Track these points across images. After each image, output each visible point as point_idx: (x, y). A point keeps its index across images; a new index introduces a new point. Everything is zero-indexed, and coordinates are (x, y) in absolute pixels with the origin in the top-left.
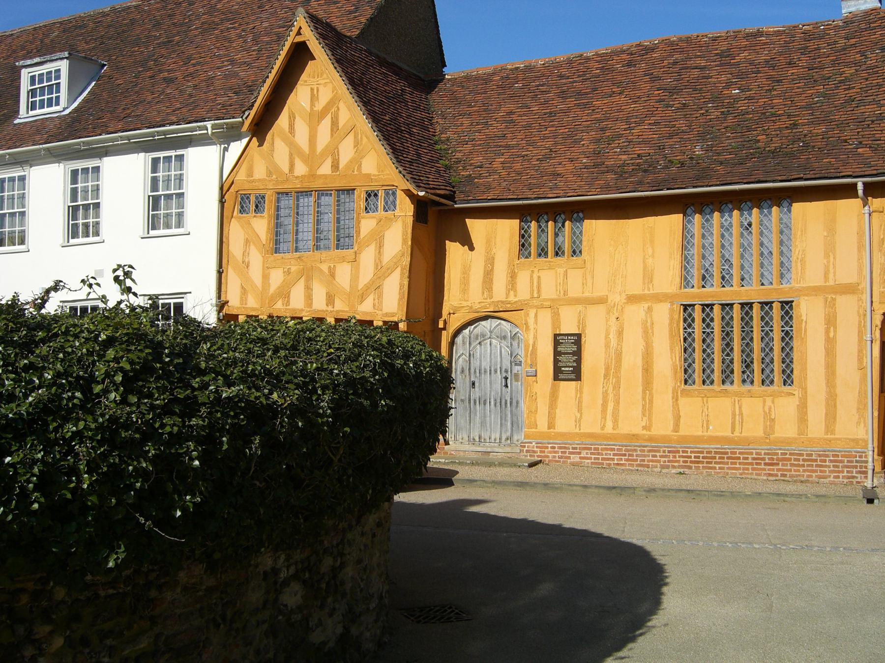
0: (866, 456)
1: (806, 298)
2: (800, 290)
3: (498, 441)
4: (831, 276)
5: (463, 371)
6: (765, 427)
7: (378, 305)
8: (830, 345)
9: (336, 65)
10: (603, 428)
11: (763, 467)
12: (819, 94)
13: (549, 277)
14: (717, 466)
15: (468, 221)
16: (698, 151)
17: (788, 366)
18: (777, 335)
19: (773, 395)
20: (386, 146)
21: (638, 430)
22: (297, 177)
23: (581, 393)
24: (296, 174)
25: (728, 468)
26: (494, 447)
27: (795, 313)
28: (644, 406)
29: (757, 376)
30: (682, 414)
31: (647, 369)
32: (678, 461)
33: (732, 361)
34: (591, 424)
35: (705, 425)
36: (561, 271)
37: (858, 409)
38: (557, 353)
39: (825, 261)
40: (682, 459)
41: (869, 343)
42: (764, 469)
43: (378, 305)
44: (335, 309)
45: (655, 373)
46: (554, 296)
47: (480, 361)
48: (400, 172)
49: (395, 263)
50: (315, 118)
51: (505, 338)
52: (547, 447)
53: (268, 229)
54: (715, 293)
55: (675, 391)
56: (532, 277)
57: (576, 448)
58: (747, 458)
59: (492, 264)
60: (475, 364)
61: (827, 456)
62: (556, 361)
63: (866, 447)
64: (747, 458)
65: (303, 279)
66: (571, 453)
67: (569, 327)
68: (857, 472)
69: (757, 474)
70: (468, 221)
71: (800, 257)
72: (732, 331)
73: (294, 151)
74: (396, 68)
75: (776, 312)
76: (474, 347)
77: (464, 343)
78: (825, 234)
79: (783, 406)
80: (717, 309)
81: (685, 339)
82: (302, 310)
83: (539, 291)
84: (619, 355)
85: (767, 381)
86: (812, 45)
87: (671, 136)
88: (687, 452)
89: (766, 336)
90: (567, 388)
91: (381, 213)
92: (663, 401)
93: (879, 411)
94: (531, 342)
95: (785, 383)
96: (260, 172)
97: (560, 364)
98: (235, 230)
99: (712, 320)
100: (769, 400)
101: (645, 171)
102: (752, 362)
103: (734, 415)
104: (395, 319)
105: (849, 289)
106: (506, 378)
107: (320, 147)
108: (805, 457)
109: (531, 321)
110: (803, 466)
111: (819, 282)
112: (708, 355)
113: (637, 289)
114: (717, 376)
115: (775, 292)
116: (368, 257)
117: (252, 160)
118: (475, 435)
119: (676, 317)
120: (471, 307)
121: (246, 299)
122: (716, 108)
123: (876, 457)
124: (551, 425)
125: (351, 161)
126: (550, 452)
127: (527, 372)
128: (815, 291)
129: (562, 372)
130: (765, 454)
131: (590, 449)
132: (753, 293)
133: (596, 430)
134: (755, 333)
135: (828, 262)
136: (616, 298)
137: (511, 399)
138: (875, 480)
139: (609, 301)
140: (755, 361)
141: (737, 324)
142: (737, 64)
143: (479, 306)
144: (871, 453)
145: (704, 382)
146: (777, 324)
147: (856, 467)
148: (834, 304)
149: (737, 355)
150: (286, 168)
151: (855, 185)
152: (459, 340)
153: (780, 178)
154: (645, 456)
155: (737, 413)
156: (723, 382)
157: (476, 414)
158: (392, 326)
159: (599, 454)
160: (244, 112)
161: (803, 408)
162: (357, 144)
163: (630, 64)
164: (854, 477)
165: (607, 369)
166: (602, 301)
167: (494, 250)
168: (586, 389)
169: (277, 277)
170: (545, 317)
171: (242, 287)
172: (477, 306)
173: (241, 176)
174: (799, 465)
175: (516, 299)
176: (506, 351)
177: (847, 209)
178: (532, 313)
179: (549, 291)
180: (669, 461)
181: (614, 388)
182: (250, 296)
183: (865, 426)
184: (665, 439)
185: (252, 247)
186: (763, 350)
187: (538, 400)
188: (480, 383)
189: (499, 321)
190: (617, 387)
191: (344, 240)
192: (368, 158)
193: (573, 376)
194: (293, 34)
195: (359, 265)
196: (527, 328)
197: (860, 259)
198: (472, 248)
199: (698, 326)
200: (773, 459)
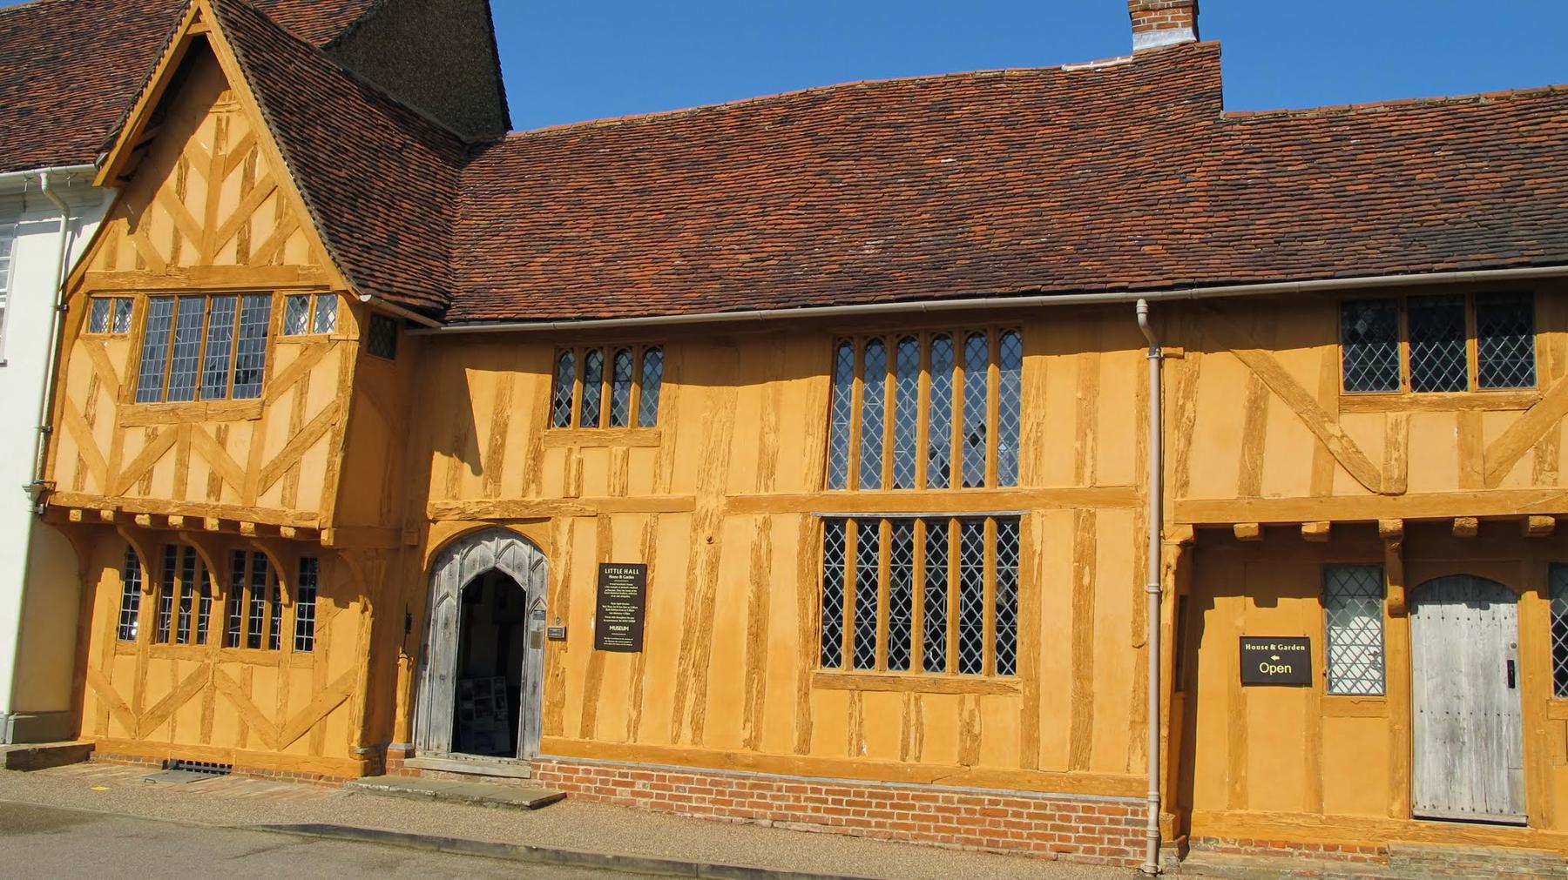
0: (1145, 813)
1: (1042, 511)
2: (1031, 497)
7: (288, 499)
8: (1083, 597)
9: (248, 72)
10: (676, 739)
12: (1084, 164)
13: (596, 462)
14: (873, 821)
17: (1007, 637)
19: (981, 690)
20: (315, 214)
21: (736, 747)
22: (182, 270)
24: (181, 265)
31: (757, 635)
32: (804, 809)
36: (618, 450)
38: (602, 599)
39: (1078, 445)
41: (1153, 598)
42: (958, 831)
43: (288, 499)
44: (222, 502)
46: (606, 497)
50: (219, 169)
52: (577, 771)
54: (883, 499)
55: (804, 676)
56: (568, 459)
57: (626, 775)
59: (503, 435)
61: (1074, 809)
62: (600, 614)
65: (175, 448)
66: (617, 783)
67: (626, 552)
68: (1127, 843)
74: (401, 108)
75: (989, 537)
77: (451, 574)
79: (998, 709)
80: (884, 528)
81: (827, 582)
82: (169, 503)
83: (578, 486)
84: (710, 601)
86: (1079, 94)
87: (829, 226)
90: (618, 663)
93: (1170, 728)
94: (560, 578)
95: (1001, 669)
97: (607, 619)
98: (80, 360)
100: (970, 702)
102: (944, 629)
104: (315, 525)
105: (1123, 497)
107: (223, 217)
108: (1032, 810)
109: (563, 540)
110: (1028, 826)
111: (1068, 484)
115: (988, 500)
116: (281, 412)
117: (116, 239)
119: (811, 540)
122: (911, 185)
123: (1163, 813)
124: (587, 731)
125: (268, 244)
128: (1059, 498)
131: (649, 777)
132: (952, 500)
133: (665, 743)
134: (949, 573)
135: (1084, 446)
136: (711, 503)
140: (948, 626)
141: (918, 556)
142: (957, 122)
144: (1153, 808)
146: (989, 557)
147: (1126, 833)
148: (1093, 525)
151: (1133, 305)
153: (998, 290)
158: (309, 536)
159: (664, 788)
161: (1031, 714)
162: (279, 215)
163: (785, 120)
164: (1122, 852)
165: (688, 632)
167: (508, 411)
168: (648, 669)
169: (135, 442)
170: (587, 531)
173: (97, 266)
175: (540, 499)
178: (565, 528)
179: (596, 488)
180: (787, 808)
182: (90, 475)
184: (782, 765)
191: (249, 378)
193: (628, 642)
194: (186, 21)
196: (556, 551)
199: (850, 556)
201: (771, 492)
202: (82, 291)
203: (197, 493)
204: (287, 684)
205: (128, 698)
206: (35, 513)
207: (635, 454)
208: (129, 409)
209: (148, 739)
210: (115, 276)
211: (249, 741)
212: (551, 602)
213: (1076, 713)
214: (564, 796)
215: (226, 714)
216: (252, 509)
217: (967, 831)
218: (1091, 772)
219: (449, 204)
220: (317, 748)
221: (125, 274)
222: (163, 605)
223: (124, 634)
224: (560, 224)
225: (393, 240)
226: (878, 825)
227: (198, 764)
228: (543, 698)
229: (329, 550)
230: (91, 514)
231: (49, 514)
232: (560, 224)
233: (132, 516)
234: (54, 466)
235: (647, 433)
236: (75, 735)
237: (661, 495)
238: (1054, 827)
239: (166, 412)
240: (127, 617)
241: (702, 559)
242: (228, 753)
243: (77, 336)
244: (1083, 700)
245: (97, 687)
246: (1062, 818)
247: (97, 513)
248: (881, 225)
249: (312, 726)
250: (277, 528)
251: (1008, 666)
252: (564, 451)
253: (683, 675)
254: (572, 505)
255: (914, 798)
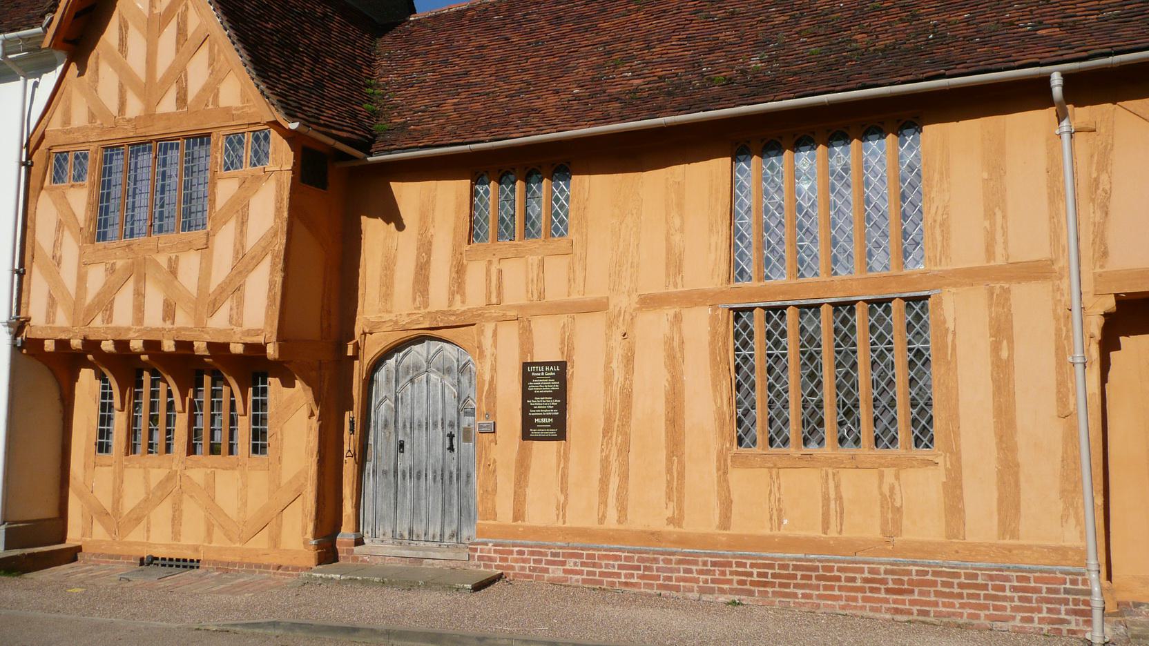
1: (953, 290)
3: (438, 539)
4: (999, 249)
5: (386, 426)
6: (884, 523)
8: (1002, 373)
10: (602, 520)
11: (883, 595)
13: (516, 272)
14: (800, 592)
15: (394, 186)
16: (755, 62)
17: (922, 412)
18: (900, 357)
19: (897, 465)
20: (242, 51)
22: (129, 121)
23: (566, 459)
25: (820, 597)
26: (429, 549)
27: (930, 317)
28: (669, 483)
29: (867, 431)
30: (735, 496)
31: (674, 420)
32: (730, 582)
33: (819, 405)
34: (582, 514)
35: (775, 517)
36: (534, 259)
37: (1063, 492)
38: (527, 395)
39: (987, 224)
40: (736, 578)
42: (887, 601)
44: (176, 326)
45: (688, 424)
47: (413, 408)
48: (258, 86)
49: (264, 248)
51: (448, 371)
52: (511, 552)
53: (89, 203)
55: (721, 458)
56: (488, 271)
57: (556, 555)
58: (853, 580)
60: (404, 413)
61: (1007, 579)
62: (526, 408)
63: (1083, 562)
64: (853, 580)
65: (132, 279)
66: (549, 563)
67: (546, 351)
68: (1067, 612)
69: (872, 609)
70: (394, 186)
71: (939, 219)
72: (818, 353)
73: (126, 80)
76: (404, 387)
77: (388, 380)
78: (985, 175)
79: (918, 484)
81: (738, 368)
82: (129, 329)
83: (499, 294)
84: (627, 397)
85: (886, 439)
87: (711, 51)
88: (744, 565)
89: (880, 359)
90: (545, 451)
91: (247, 169)
92: (702, 473)
94: (487, 377)
96: (79, 118)
97: (532, 413)
99: (783, 334)
101: (669, 94)
102: (856, 406)
103: (826, 499)
104: (260, 340)
105: (1038, 271)
106: (451, 436)
107: (161, 70)
108: (963, 580)
109: (487, 342)
110: (960, 596)
111: (977, 260)
112: (778, 395)
113: (655, 284)
114: (794, 430)
116: (224, 240)
117: (69, 99)
118: (403, 528)
119: (722, 329)
120: (396, 323)
121: (54, 314)
122: (782, 12)
124: (518, 515)
125: (204, 90)
126: (516, 561)
127: (480, 426)
128: (970, 276)
129: (535, 426)
130: (886, 572)
131: (580, 556)
133: (591, 523)
135: (993, 225)
136: (623, 302)
137: (459, 470)
138: (1107, 629)
139: (611, 307)
140: (862, 404)
143: (407, 320)
145: (771, 442)
146: (899, 338)
147: (1066, 602)
148: (1007, 299)
149: (828, 394)
150: (113, 108)
151: (1046, 80)
152: (381, 375)
154: (671, 570)
155: (832, 495)
156: (806, 441)
157: (405, 494)
159: (594, 565)
160: (43, 17)
161: (954, 489)
164: (1062, 621)
165: (609, 420)
166: (599, 306)
167: (432, 231)
168: (574, 456)
169: (97, 278)
170: (510, 335)
171: (51, 296)
172: (404, 321)
173: (55, 124)
174: (951, 595)
176: (451, 391)
177: (1026, 128)
178: (489, 328)
179: (515, 294)
180: (713, 581)
181: (620, 452)
183: (1078, 523)
184: (705, 540)
185: (67, 234)
186: (875, 384)
187: (498, 472)
188: (412, 445)
189: (441, 344)
190: (624, 450)
191: (191, 215)
192: (229, 88)
193: (553, 433)
195: (211, 253)
196: (482, 354)
197: (1054, 216)
198: (400, 227)
199: (759, 345)
200: (901, 582)
201: (680, 289)
202: (43, 147)
203: (154, 318)
204: (245, 486)
205: (107, 503)
206: (14, 347)
207: (549, 262)
208: (90, 248)
209: (126, 539)
210: (70, 132)
211: (215, 537)
212: (480, 400)
213: (1002, 483)
214: (500, 577)
215: (193, 515)
216: (203, 329)
217: (895, 602)
218: (1023, 542)
219: (369, 66)
220: (275, 541)
221: (79, 129)
222: (133, 421)
223: (103, 448)
224: (466, 74)
225: (319, 84)
226: (804, 596)
227: (171, 560)
228: (477, 487)
229: (275, 362)
230: (62, 344)
231: (27, 349)
232: (466, 74)
233: (98, 342)
234: (28, 304)
235: (559, 243)
236: (63, 540)
237: (575, 297)
238: (987, 597)
239: (123, 248)
240: (104, 434)
241: (618, 354)
242: (196, 549)
243: (42, 188)
244: (1009, 471)
245: (81, 496)
246: (995, 588)
247: (127, 343)
248: (760, 45)
249: (270, 522)
250: (226, 346)
251: (925, 440)
252: (483, 264)
253: (605, 464)
254: (495, 312)
255: (840, 569)
